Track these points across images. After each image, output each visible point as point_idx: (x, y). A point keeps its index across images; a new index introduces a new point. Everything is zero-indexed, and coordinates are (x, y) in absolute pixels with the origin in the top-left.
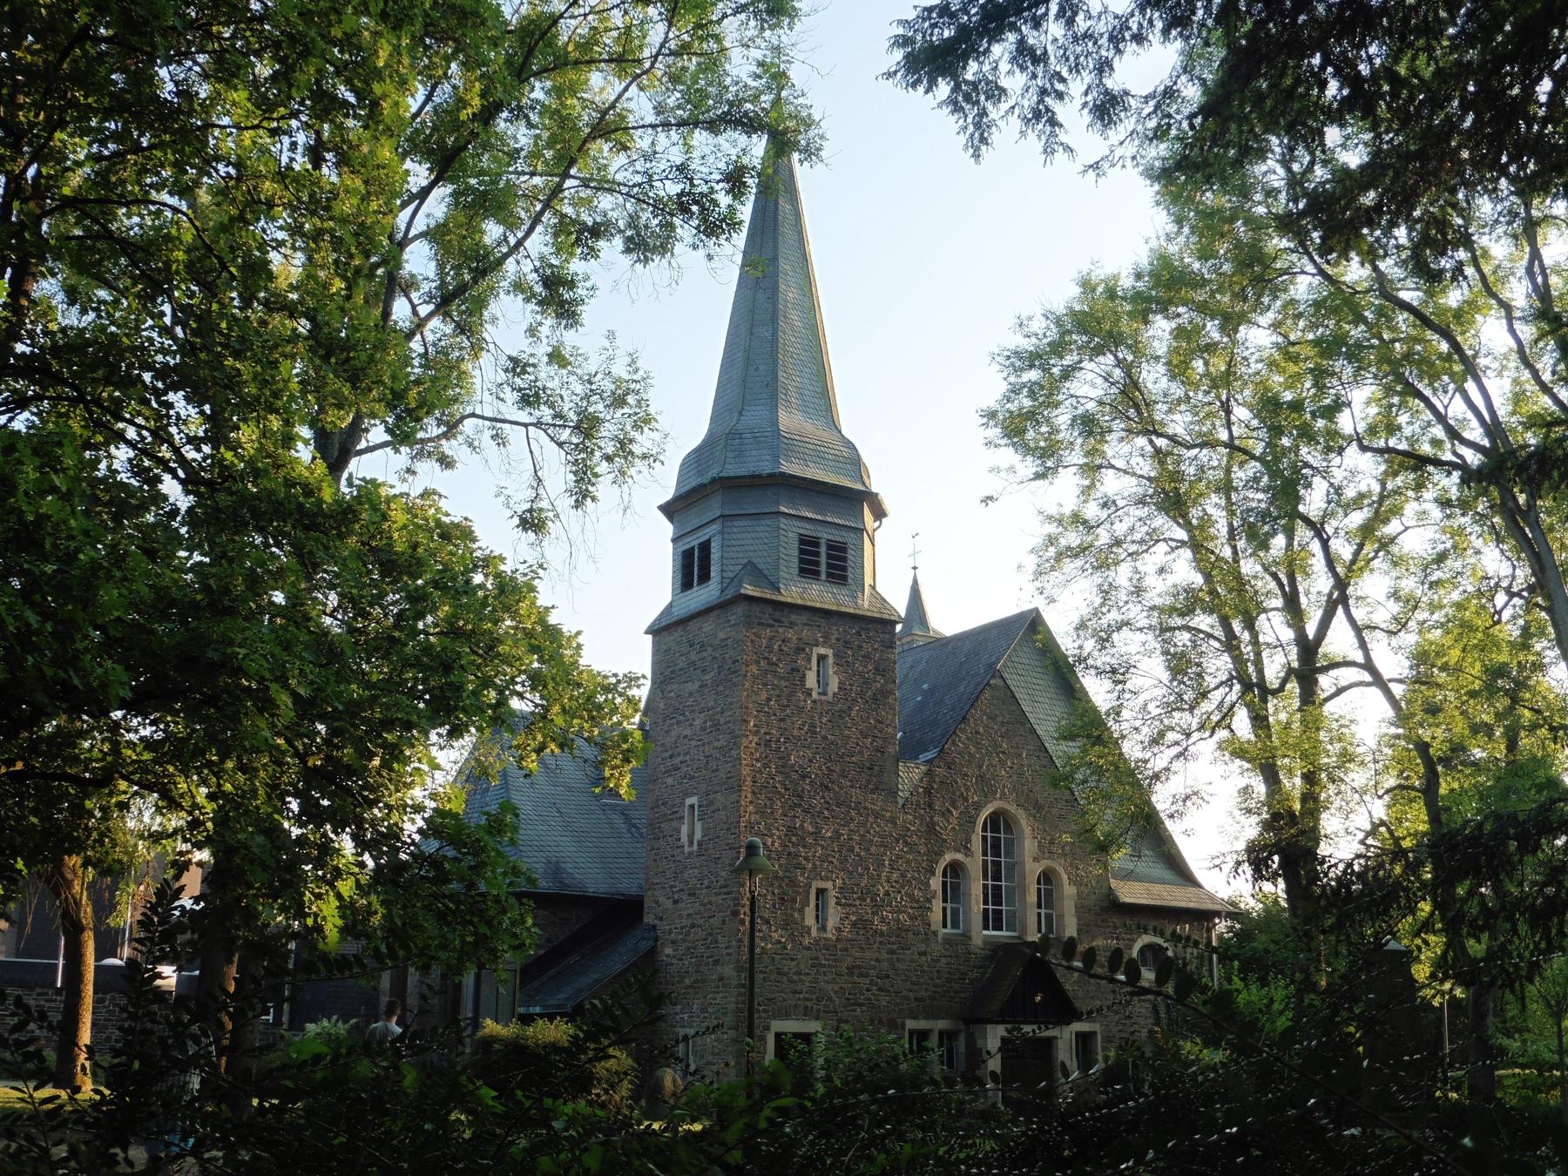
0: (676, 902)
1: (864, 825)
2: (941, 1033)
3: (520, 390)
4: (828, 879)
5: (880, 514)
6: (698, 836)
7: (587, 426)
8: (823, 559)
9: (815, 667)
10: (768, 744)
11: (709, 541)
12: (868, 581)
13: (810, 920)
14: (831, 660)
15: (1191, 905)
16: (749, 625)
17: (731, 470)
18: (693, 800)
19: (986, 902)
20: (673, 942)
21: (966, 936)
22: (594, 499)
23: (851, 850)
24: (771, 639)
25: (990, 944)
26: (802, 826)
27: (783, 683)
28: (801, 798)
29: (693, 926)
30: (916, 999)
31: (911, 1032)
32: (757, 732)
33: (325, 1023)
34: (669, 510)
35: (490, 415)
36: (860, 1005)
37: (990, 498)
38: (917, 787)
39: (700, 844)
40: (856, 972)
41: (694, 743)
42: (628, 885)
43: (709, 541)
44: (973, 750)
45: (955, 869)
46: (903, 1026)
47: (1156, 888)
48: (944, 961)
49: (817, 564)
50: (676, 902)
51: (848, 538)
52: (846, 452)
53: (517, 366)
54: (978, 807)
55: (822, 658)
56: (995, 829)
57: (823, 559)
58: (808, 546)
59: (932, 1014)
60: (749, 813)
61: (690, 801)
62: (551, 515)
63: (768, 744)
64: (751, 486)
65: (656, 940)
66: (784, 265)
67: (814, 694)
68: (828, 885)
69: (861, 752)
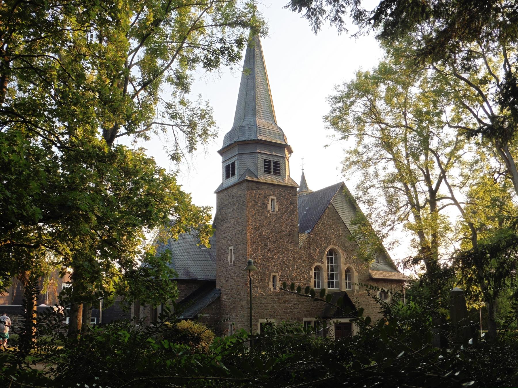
0: (227, 281)
1: (288, 254)
3: (170, 114)
4: (276, 272)
5: (290, 152)
6: (233, 259)
7: (193, 125)
8: (272, 167)
9: (270, 203)
10: (255, 229)
12: (287, 174)
13: (271, 286)
14: (276, 200)
15: (396, 278)
16: (248, 190)
17: (241, 139)
18: (231, 248)
19: (328, 279)
20: (226, 294)
22: (195, 149)
23: (284, 262)
24: (255, 194)
27: (260, 208)
28: (267, 246)
29: (232, 289)
30: (306, 311)
31: (305, 322)
34: (221, 152)
35: (161, 123)
37: (327, 146)
38: (305, 241)
39: (234, 262)
40: (286, 302)
41: (231, 229)
42: (211, 276)
44: (323, 229)
45: (318, 268)
46: (302, 320)
47: (385, 273)
49: (270, 169)
51: (281, 160)
52: (279, 132)
53: (169, 106)
54: (325, 248)
55: (272, 200)
56: (331, 255)
57: (272, 167)
58: (267, 163)
59: (311, 316)
60: (250, 251)
61: (230, 248)
62: (181, 155)
65: (221, 294)
66: (257, 70)
67: (270, 212)
68: (277, 274)
69: (286, 231)
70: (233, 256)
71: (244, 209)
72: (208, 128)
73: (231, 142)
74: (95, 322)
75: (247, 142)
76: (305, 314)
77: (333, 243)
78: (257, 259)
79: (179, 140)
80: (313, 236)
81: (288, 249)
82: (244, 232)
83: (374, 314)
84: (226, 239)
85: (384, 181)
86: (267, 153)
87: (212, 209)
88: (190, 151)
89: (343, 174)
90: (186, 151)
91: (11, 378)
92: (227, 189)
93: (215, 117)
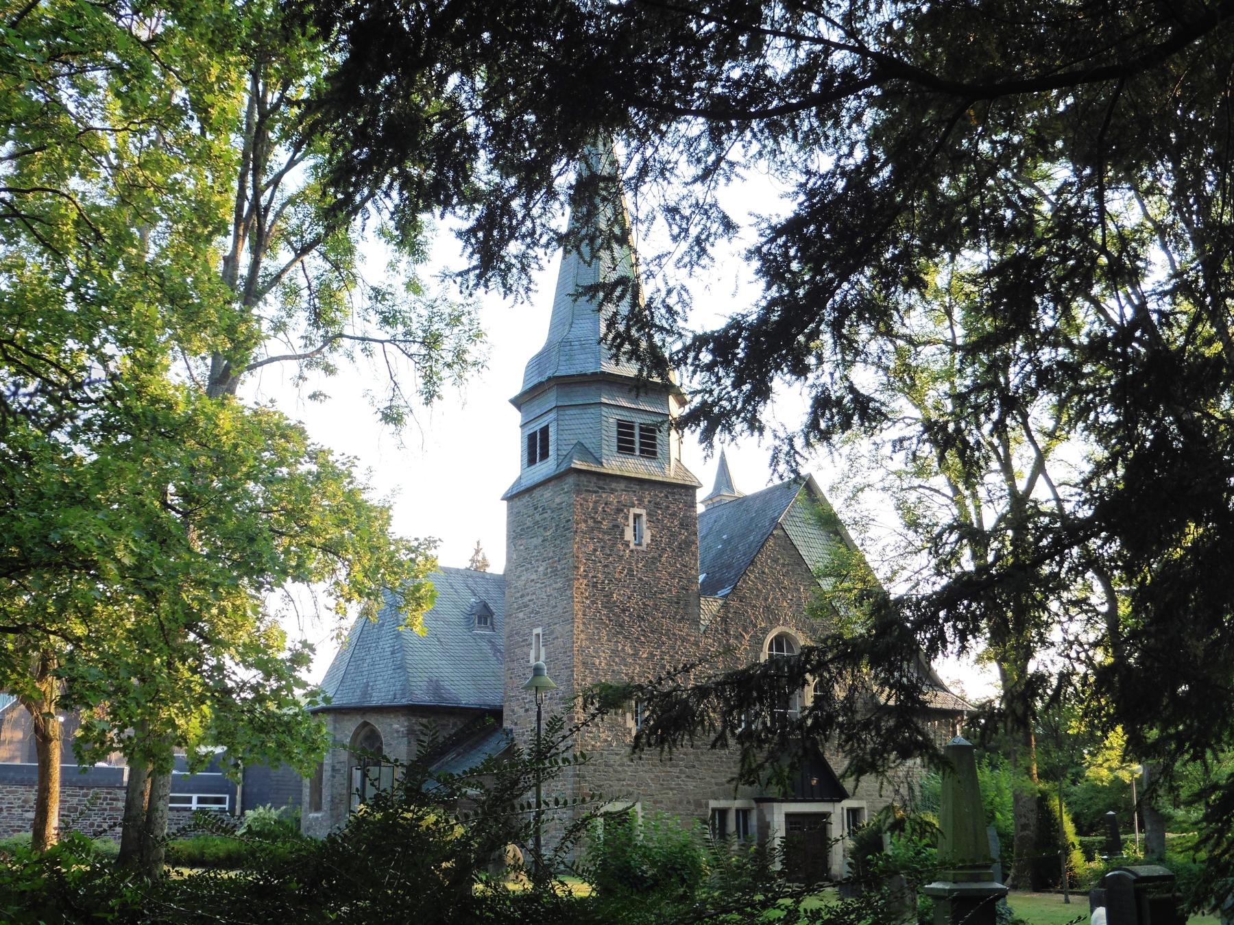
0: (527, 710)
2: (737, 811)
3: (382, 313)
7: (432, 341)
8: (637, 439)
9: (632, 524)
10: (595, 586)
12: (674, 455)
14: (644, 518)
16: (578, 492)
17: (563, 371)
18: (539, 630)
24: (596, 502)
26: (623, 649)
27: (607, 537)
30: (717, 784)
31: (714, 810)
32: (586, 577)
33: (261, 809)
34: (518, 402)
35: (360, 335)
36: (671, 789)
38: (715, 617)
42: (492, 699)
44: (760, 587)
46: (707, 805)
49: (632, 442)
50: (527, 710)
53: (378, 295)
54: (765, 631)
55: (637, 517)
57: (637, 439)
58: (624, 429)
61: (535, 631)
64: (599, 381)
67: (632, 546)
70: (543, 650)
71: (568, 539)
72: (470, 347)
73: (540, 379)
74: (226, 806)
75: (578, 379)
76: (713, 792)
78: (599, 657)
81: (674, 634)
82: (568, 592)
84: (528, 610)
87: (438, 543)
88: (428, 401)
90: (417, 401)
91: (944, 880)
92: (530, 490)
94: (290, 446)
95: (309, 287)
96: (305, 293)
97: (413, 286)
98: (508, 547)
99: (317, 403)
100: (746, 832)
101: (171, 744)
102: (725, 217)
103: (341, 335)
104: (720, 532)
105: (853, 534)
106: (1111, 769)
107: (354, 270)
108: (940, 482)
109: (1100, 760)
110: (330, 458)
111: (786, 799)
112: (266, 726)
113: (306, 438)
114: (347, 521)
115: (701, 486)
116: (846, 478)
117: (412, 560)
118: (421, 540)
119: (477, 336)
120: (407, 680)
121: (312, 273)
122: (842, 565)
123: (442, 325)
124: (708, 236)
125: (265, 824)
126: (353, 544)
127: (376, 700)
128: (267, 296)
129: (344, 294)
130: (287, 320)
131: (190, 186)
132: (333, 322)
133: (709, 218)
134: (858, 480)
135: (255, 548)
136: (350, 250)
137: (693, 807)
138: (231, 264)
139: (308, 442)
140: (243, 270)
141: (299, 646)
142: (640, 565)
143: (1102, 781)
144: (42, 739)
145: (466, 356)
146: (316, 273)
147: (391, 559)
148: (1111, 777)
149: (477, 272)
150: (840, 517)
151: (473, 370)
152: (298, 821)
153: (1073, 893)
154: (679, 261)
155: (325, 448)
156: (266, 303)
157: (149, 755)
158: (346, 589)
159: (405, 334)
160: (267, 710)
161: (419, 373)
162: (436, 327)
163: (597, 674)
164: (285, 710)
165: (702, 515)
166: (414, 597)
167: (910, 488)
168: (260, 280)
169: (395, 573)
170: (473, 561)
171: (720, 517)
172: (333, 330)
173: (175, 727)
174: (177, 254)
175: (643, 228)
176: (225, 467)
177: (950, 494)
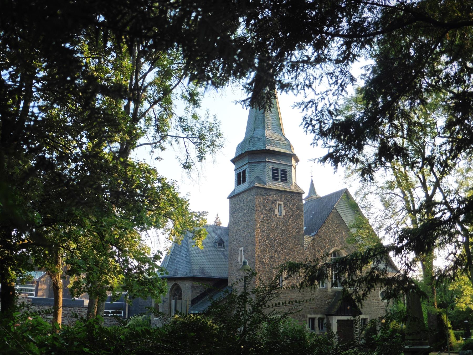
1: (294, 255)
2: (319, 319)
3: (183, 127)
5: (297, 161)
7: (202, 137)
8: (280, 175)
10: (263, 231)
11: (245, 170)
12: (294, 181)
14: (283, 205)
16: (257, 195)
17: (251, 149)
18: (242, 248)
21: (326, 289)
22: (205, 159)
24: (264, 199)
25: (334, 291)
26: (274, 256)
27: (268, 213)
28: (274, 247)
30: (311, 308)
31: (309, 319)
32: (260, 228)
34: (234, 161)
35: (175, 135)
38: (310, 243)
41: (242, 231)
42: (223, 275)
43: (245, 170)
48: (319, 296)
49: (278, 176)
51: (288, 168)
52: (286, 142)
53: (181, 120)
57: (280, 175)
58: (275, 171)
59: (316, 313)
60: (258, 252)
61: (240, 249)
62: (192, 164)
63: (263, 231)
67: (278, 216)
69: (292, 233)
74: (122, 315)
76: (309, 311)
77: (337, 245)
78: (265, 259)
79: (190, 150)
80: (317, 238)
82: (253, 234)
83: (375, 312)
85: (382, 188)
86: (275, 162)
88: (200, 160)
89: (345, 181)
90: (196, 160)
92: (238, 195)
93: (223, 129)
94: (151, 176)
95: (155, 117)
96: (154, 119)
97: (194, 117)
98: (230, 217)
99: (158, 161)
100: (322, 329)
101: (106, 290)
102: (351, 76)
103: (167, 135)
104: (311, 211)
105: (363, 211)
106: (466, 304)
107: (172, 111)
108: (398, 191)
109: (462, 300)
110: (166, 181)
111: (338, 314)
112: (145, 282)
113: (157, 174)
114: (173, 205)
115: (304, 193)
116: (361, 189)
117: (198, 220)
118: (201, 212)
119: (219, 135)
120: (191, 267)
121: (156, 112)
122: (360, 223)
123: (206, 131)
124: (344, 84)
125: (137, 322)
126: (176, 214)
127: (180, 275)
128: (141, 120)
129: (168, 120)
130: (147, 130)
131: (113, 79)
132: (164, 131)
133: (346, 76)
134: (366, 190)
135: (140, 214)
136: (171, 103)
137: (301, 317)
138: (127, 108)
139: (158, 175)
140: (131, 111)
141: (156, 252)
142: (281, 223)
143: (462, 309)
144: (55, 288)
145: (215, 143)
146: (157, 112)
147: (190, 219)
148: (466, 307)
149: (249, 100)
150: (359, 205)
151: (217, 148)
152: (150, 321)
153: (452, 353)
154: (334, 93)
155: (164, 177)
156: (140, 123)
157: (98, 294)
158: (173, 231)
159: (192, 135)
160: (144, 276)
161: (197, 150)
162: (203, 132)
163: (264, 265)
164: (151, 277)
165: (304, 204)
166: (197, 234)
167: (387, 193)
168: (138, 114)
169: (191, 225)
170: (215, 222)
171: (311, 205)
172: (165, 133)
173: (108, 283)
174: (109, 104)
175: (318, 81)
176: (128, 184)
177: (402, 196)
